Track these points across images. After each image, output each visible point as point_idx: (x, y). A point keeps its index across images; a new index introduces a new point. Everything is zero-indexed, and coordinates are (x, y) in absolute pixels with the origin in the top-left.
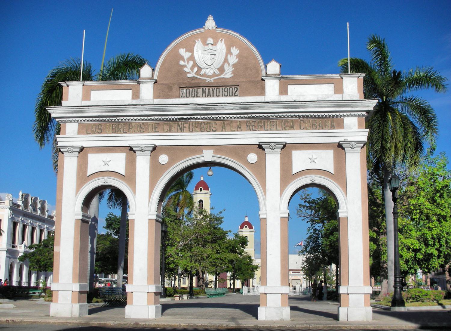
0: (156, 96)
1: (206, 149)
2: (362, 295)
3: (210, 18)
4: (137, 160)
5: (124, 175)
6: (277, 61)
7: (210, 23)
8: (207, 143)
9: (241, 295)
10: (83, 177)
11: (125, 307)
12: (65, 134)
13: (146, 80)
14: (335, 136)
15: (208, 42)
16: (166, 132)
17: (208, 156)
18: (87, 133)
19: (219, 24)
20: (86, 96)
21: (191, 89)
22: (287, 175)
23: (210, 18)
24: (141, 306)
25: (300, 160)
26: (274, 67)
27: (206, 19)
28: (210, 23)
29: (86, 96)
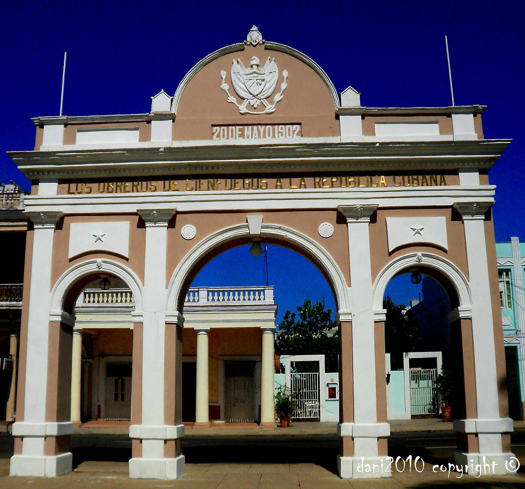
0: (176, 136)
1: (76, 221)
2: (498, 435)
3: (254, 28)
4: (20, 474)
5: (127, 256)
6: (358, 88)
7: (255, 35)
8: (257, 209)
9: (335, 478)
10: (61, 260)
11: (127, 461)
12: (36, 194)
13: (162, 117)
14: (446, 194)
15: (252, 62)
16: (192, 190)
17: (256, 226)
18: (69, 193)
19: (265, 37)
20: (69, 139)
21: (225, 128)
22: (382, 253)
23: (254, 28)
24: (154, 458)
25: (400, 230)
26: (351, 98)
27: (248, 30)
28: (255, 35)
29: (69, 139)
